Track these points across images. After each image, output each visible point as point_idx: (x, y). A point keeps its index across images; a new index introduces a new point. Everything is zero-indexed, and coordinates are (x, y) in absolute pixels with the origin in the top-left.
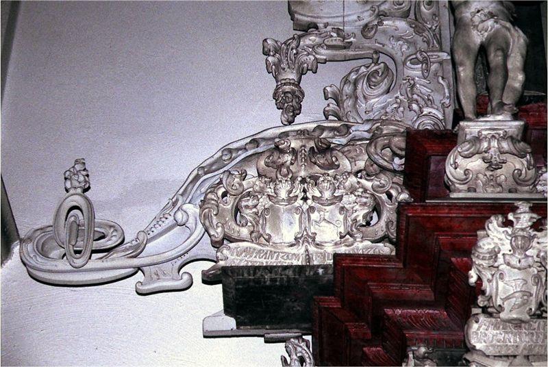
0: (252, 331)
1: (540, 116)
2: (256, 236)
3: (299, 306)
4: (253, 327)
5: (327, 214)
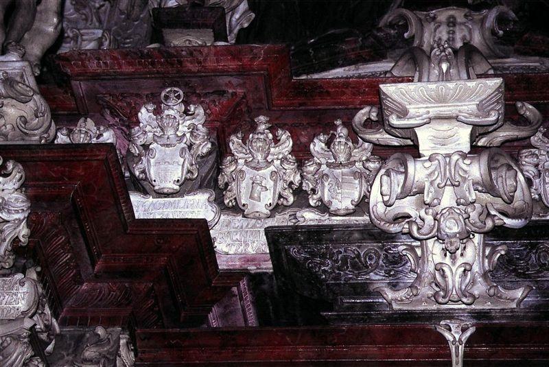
1: (83, 65)
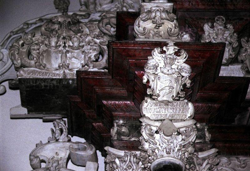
0: (36, 115)
1: (182, 4)
2: (39, 65)
3: (60, 101)
4: (36, 113)
5: (75, 54)
